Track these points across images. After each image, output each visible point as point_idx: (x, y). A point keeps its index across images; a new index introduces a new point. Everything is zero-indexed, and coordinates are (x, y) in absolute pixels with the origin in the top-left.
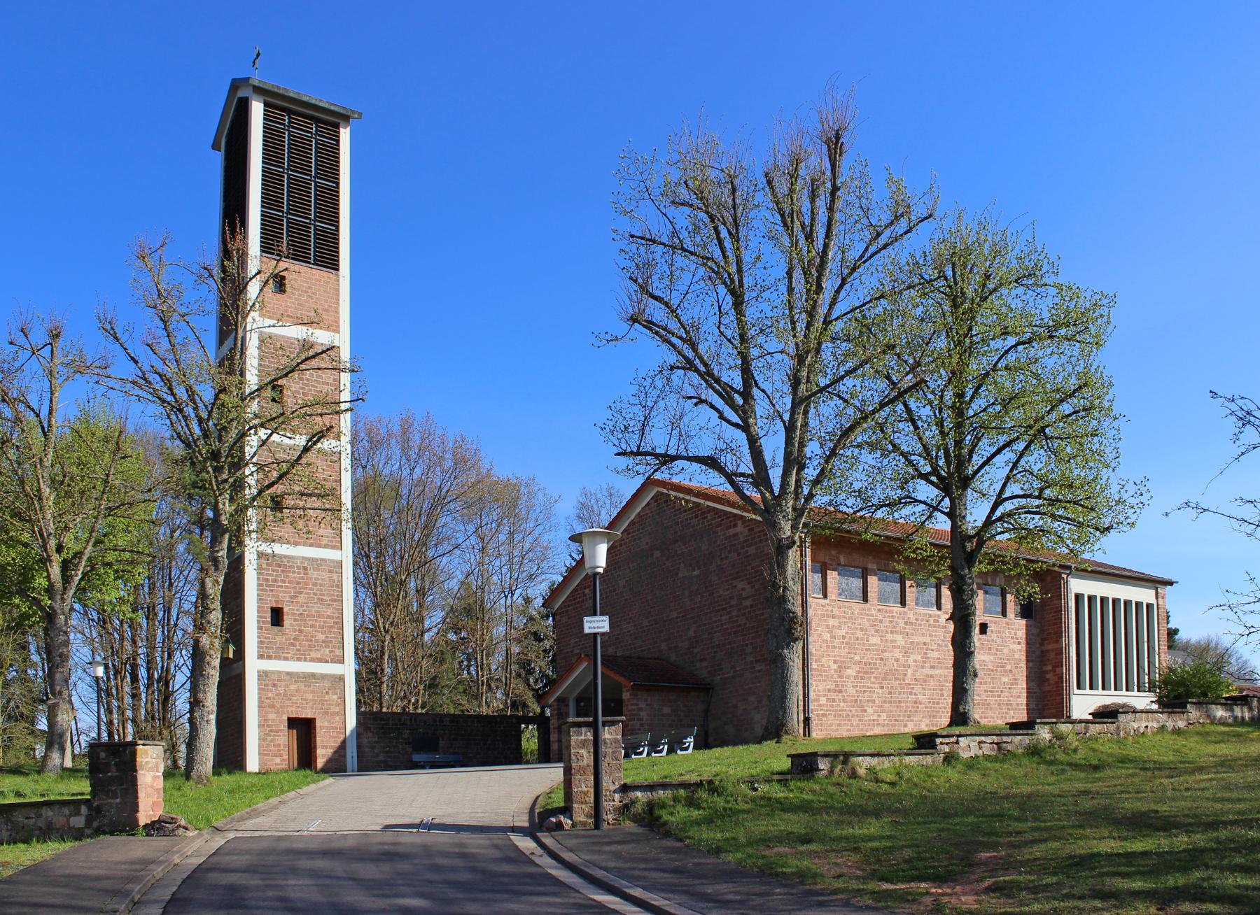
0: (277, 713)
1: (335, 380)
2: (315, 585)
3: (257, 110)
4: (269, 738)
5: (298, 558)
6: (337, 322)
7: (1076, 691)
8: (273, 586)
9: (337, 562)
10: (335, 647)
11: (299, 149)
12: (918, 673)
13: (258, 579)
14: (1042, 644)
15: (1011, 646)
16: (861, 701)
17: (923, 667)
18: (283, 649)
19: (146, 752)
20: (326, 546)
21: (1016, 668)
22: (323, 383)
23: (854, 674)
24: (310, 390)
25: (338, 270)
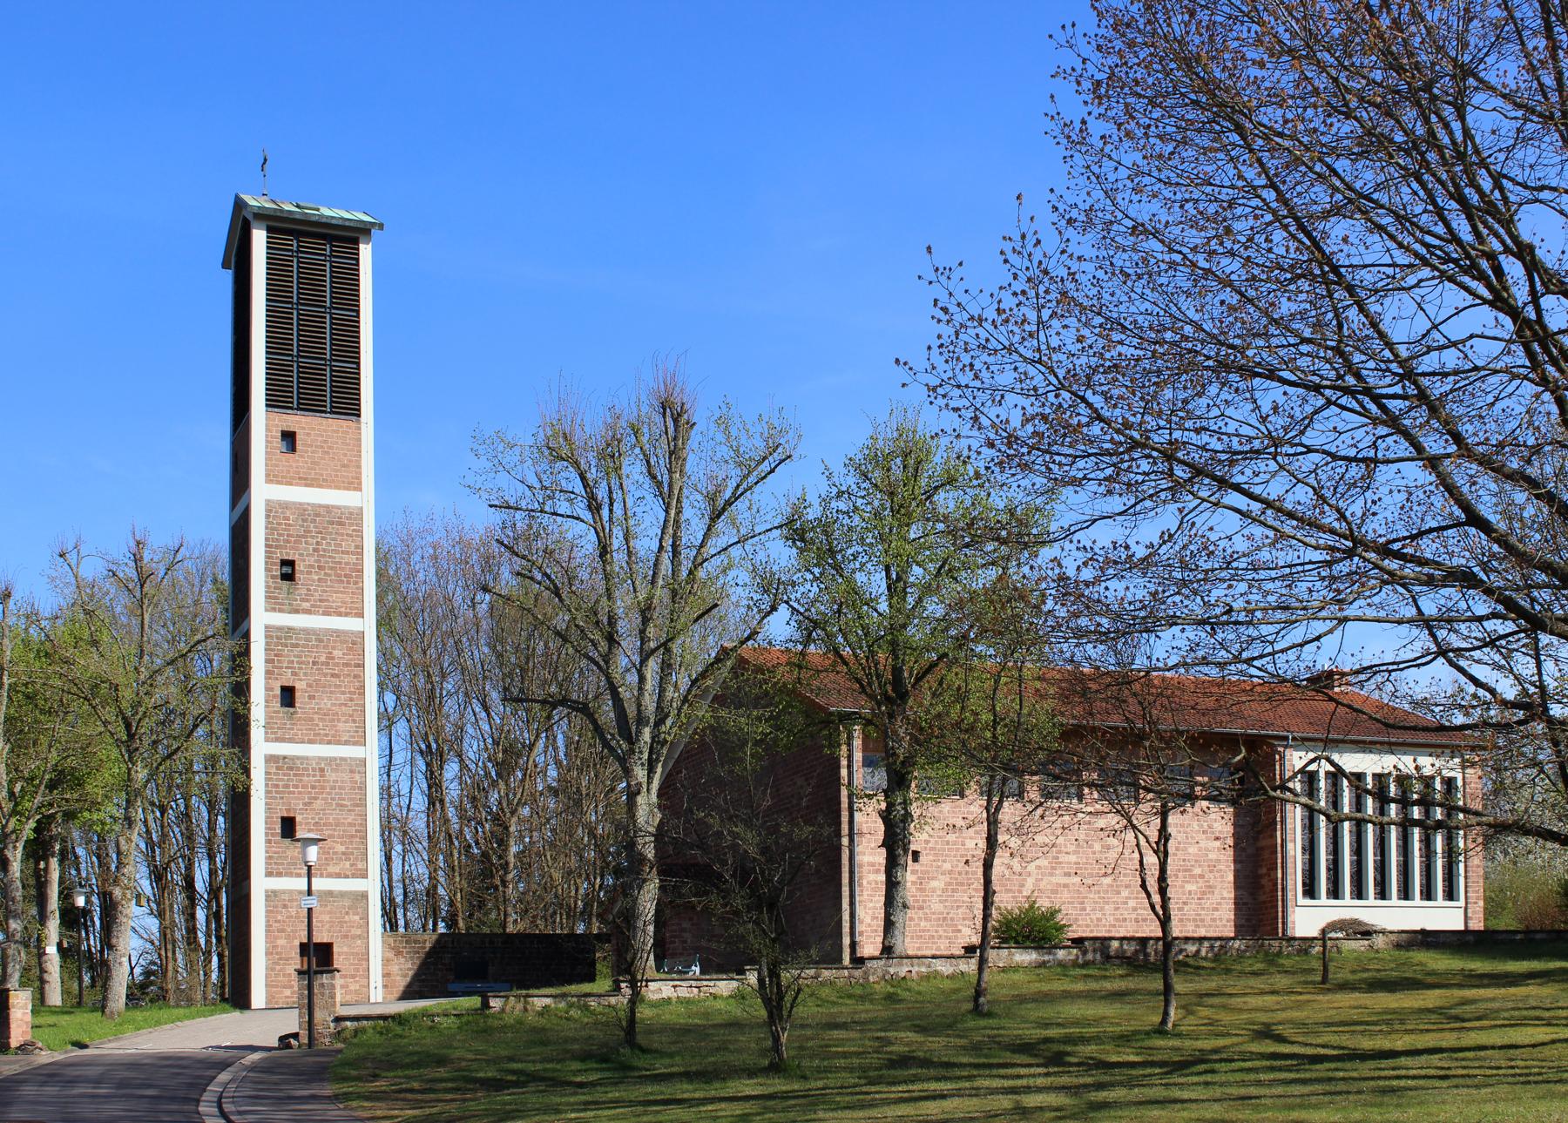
0: (288, 937)
1: (357, 547)
2: (333, 788)
3: (259, 238)
4: (278, 968)
5: (314, 758)
6: (359, 478)
7: (1301, 900)
8: (284, 792)
9: (360, 760)
10: (356, 859)
11: (311, 281)
12: (1044, 883)
13: (267, 785)
14: (1256, 839)
15: (1203, 844)
16: (952, 919)
17: (1051, 875)
18: (295, 864)
19: (17, 996)
20: (346, 743)
21: (1211, 871)
22: (343, 552)
23: (942, 885)
24: (327, 562)
25: (359, 416)
